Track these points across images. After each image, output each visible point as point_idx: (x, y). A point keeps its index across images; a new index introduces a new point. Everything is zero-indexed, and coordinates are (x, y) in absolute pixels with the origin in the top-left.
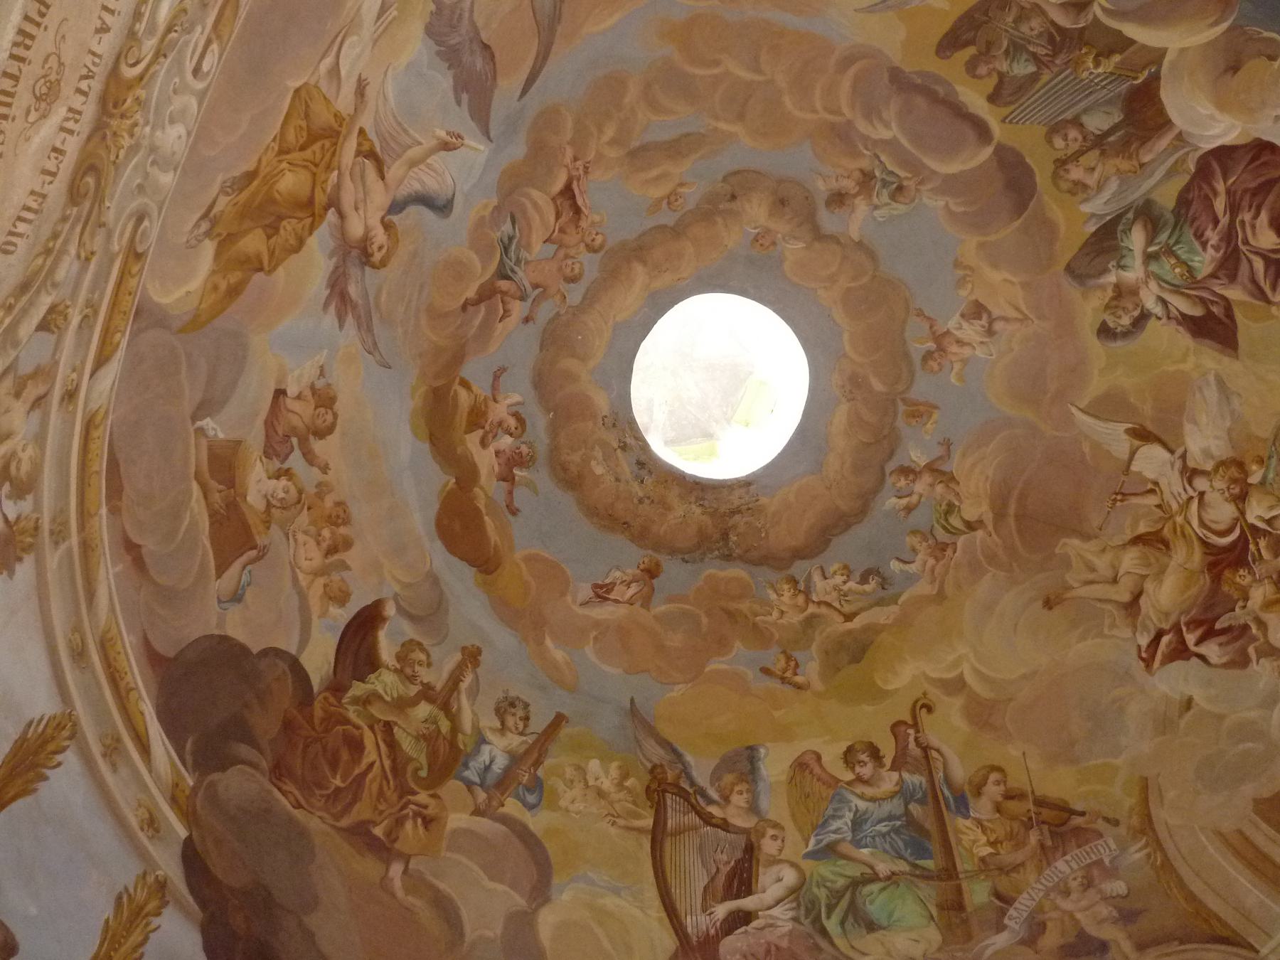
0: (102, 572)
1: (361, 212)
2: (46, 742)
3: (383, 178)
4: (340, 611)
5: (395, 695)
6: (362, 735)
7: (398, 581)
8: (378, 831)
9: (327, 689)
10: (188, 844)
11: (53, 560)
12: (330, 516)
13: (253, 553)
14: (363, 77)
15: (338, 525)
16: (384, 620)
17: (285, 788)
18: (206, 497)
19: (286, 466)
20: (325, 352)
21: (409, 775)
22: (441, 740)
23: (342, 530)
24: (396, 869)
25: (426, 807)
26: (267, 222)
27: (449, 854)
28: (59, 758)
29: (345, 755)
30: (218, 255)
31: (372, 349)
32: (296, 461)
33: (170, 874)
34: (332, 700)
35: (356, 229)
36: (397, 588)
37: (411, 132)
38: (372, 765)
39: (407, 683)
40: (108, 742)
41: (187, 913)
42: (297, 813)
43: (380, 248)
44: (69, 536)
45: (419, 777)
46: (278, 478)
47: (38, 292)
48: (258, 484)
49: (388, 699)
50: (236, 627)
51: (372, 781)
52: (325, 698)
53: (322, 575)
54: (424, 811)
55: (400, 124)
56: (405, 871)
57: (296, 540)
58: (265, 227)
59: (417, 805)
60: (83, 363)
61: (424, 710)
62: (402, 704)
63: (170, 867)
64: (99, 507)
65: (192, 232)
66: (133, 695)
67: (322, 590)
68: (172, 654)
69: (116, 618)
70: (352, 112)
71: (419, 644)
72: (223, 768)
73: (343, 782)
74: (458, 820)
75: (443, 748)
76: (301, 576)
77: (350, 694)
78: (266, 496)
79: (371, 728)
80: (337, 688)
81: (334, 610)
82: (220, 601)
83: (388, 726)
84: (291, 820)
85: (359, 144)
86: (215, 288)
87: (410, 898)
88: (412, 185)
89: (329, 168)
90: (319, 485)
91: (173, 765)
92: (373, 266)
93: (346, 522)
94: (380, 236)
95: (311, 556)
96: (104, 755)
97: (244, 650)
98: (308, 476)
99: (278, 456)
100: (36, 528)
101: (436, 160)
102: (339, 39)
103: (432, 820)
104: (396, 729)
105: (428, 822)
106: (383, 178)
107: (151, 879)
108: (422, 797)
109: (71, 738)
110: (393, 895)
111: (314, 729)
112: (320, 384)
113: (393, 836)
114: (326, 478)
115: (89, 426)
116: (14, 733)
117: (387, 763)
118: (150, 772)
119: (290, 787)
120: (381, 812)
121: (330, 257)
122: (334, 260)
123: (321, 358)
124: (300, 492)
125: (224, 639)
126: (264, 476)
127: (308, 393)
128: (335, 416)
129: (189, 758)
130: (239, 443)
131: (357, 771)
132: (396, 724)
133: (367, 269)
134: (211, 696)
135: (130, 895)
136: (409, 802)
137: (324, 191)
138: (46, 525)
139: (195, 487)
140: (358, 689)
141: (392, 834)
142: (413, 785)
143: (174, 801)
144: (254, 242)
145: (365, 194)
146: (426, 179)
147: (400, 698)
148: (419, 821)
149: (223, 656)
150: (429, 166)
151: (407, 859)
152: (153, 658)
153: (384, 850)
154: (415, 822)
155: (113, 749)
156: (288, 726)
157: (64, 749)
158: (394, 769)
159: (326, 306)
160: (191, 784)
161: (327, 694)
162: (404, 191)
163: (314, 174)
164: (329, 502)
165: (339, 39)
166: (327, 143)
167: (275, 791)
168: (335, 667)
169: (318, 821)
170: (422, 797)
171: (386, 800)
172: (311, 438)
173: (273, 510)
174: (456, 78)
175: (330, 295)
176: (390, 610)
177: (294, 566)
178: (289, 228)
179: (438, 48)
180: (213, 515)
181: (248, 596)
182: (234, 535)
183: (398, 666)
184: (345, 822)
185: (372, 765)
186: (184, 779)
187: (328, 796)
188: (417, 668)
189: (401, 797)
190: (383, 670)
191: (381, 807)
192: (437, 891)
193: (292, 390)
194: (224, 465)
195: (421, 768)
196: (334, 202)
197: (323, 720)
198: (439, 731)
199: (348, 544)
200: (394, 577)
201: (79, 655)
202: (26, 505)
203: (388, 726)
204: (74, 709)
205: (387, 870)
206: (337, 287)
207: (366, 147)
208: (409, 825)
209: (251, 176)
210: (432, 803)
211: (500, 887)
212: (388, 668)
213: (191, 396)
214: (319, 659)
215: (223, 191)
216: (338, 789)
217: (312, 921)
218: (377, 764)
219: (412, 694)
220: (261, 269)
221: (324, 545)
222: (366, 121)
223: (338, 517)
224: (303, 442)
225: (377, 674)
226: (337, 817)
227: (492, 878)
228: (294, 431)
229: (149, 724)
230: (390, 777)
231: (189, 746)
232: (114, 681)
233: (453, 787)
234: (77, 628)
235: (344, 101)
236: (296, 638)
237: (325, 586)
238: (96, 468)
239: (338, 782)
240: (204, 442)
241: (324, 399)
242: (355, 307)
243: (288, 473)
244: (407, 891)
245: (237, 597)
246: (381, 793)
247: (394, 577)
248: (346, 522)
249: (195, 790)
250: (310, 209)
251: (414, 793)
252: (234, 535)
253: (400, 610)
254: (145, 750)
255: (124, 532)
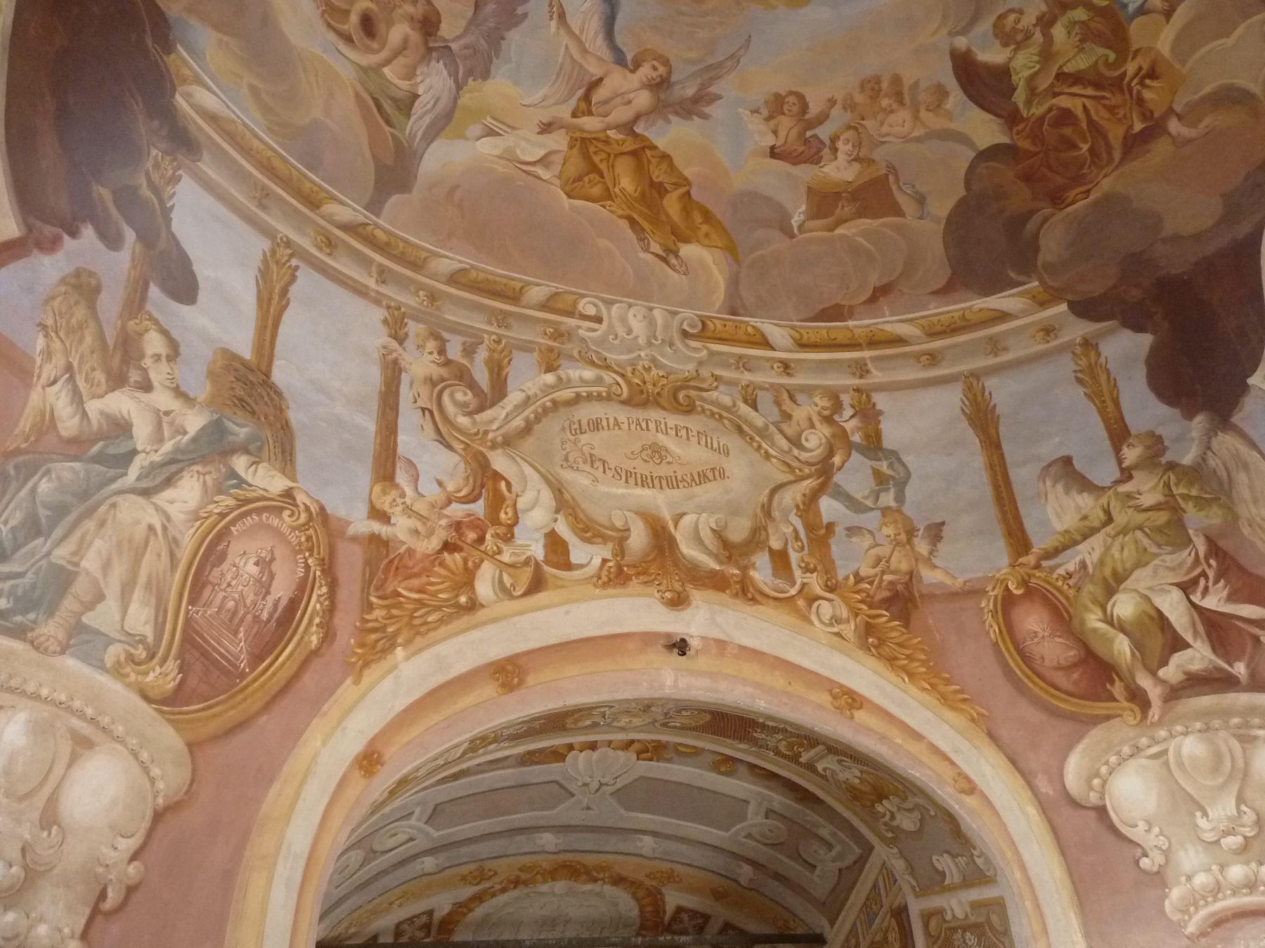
0: (888, 327)
1: (631, 96)
2: (975, 399)
3: (601, 80)
4: (951, 99)
5: (1037, 58)
6: (1059, 108)
7: (937, 30)
8: (1138, 127)
9: (1011, 129)
10: (1072, 306)
11: (877, 376)
12: (871, 97)
13: (891, 178)
14: (538, 130)
15: (880, 90)
16: (969, 51)
17: (1070, 200)
18: (845, 221)
19: (828, 142)
20: (740, 110)
21: (1108, 73)
22: (1092, 25)
23: (885, 85)
24: (1174, 126)
25: (1140, 69)
26: (656, 195)
27: (1188, 66)
28: (987, 393)
29: (1067, 131)
30: (687, 241)
31: (735, 58)
32: (824, 132)
33: (1081, 333)
34: (1021, 127)
35: (643, 99)
36: (945, 31)
37: (560, 60)
38: (1084, 106)
39: (1031, 41)
40: (989, 348)
41: (1112, 331)
42: (1092, 197)
43: (655, 69)
44: (864, 359)
45: (1113, 64)
46: (836, 150)
47: (739, 417)
48: (839, 170)
49: (1038, 67)
50: (942, 207)
51: (1097, 113)
52: (1018, 133)
53: (918, 111)
54: (1143, 72)
55: (558, 75)
56: (1179, 117)
57: (887, 135)
58: (662, 197)
59: (1134, 77)
60: (768, 359)
61: (1058, 32)
62: (1047, 54)
63: (1079, 329)
64: (847, 328)
65: (678, 272)
66: (968, 315)
67: (931, 114)
68: (949, 272)
69: (917, 319)
70: (564, 131)
71: (999, 17)
72: (1037, 250)
73: (1085, 142)
74: (1164, 42)
75: (1098, 25)
76: (916, 134)
77: (1021, 105)
78: (849, 162)
79: (1056, 95)
80: (1012, 119)
81: (949, 104)
82: (921, 218)
83: (1061, 76)
84: (1096, 203)
85: (584, 114)
86: (707, 235)
87: (1202, 125)
88: (598, 44)
89: (607, 141)
90: (845, 108)
91: (1020, 294)
92: (670, 73)
93: (877, 80)
94: (645, 71)
95: (900, 121)
96: (996, 355)
97: (962, 203)
98: (839, 117)
99: (819, 150)
100: (858, 390)
101: (574, 22)
102: (524, 167)
103: (1153, 70)
104: (1066, 70)
105: (1152, 74)
106: (601, 80)
107: (1078, 350)
108: (1131, 68)
109: (978, 379)
110: (1189, 141)
111: (1036, 154)
112: (765, 113)
113: (1148, 114)
114: (839, 102)
115: (803, 345)
116: (964, 424)
117: (1090, 91)
118: (1017, 318)
119: (1072, 194)
120: (1125, 116)
121: (669, 122)
122: (671, 117)
123: (744, 112)
124: (849, 127)
125: (949, 220)
126: (834, 164)
127: (772, 123)
128: (791, 93)
129: (1021, 278)
130: (810, 190)
131: (1084, 125)
132: (1061, 67)
133: (674, 78)
134: (987, 244)
135: (1080, 371)
136: (1129, 84)
137: (624, 141)
138: (856, 382)
139: (840, 231)
140: (1020, 97)
141: (1146, 115)
142: (1117, 73)
143: (1043, 305)
144: (672, 204)
145: (618, 96)
146: (591, 35)
147: (1040, 54)
148: (1148, 81)
149: (961, 224)
150: (582, 31)
151: (1171, 111)
152: (946, 291)
153: (1154, 129)
154: (1148, 87)
155: (995, 345)
156: (1028, 178)
157: (983, 387)
158: (1097, 86)
159: (705, 117)
160: (1037, 283)
161: (1015, 130)
162: (606, 54)
163: (616, 156)
164: (859, 98)
165: (524, 167)
166: (592, 149)
167: (1070, 209)
168: (996, 115)
169: (1106, 180)
170: (1131, 68)
171: (1118, 107)
172: (807, 117)
173: (861, 155)
174: (508, 29)
175: (696, 114)
176: (961, 42)
177: (907, 139)
178: (657, 173)
179: (495, 60)
180: (859, 215)
181: (922, 189)
182: (873, 196)
183: (1013, 47)
184: (1117, 155)
185: (1084, 106)
186: (1031, 289)
187: (1093, 162)
188: (1020, 26)
189: (1122, 92)
190: (1013, 64)
191: (1121, 115)
192: (1208, 98)
193: (770, 140)
194: (824, 202)
195: (1107, 57)
196: (628, 128)
197: (1034, 143)
198: (1083, 22)
199: (897, 80)
200: (934, 34)
201: (933, 358)
202: (846, 399)
203: (1061, 76)
204: (961, 373)
205: (1170, 135)
206: (692, 107)
207: (583, 106)
208: (1147, 95)
209: (633, 223)
210: (1139, 60)
211: (1240, 30)
212: (1011, 59)
213: (779, 243)
214: (985, 130)
215: (647, 250)
216: (1091, 150)
217: (1168, 230)
218: (1088, 103)
219: (1041, 39)
220: (688, 193)
221: (895, 106)
222: (564, 112)
223: (873, 89)
224: (811, 125)
225: (1013, 73)
226: (1111, 160)
227: (1228, 35)
228: (801, 134)
229: (991, 306)
230: (1099, 94)
231: (1013, 275)
232: (953, 330)
233: (1137, 30)
234: (917, 356)
235: (558, 141)
236: (963, 148)
237: (928, 110)
238: (824, 332)
239: (1085, 147)
240: (811, 224)
241: (776, 106)
242: (703, 86)
243: (834, 139)
244: (1193, 125)
245: (921, 200)
246: (1111, 109)
247: (934, 34)
248: (877, 80)
249: (1042, 282)
250: (641, 153)
251: (1125, 74)
252: (873, 196)
253: (964, 32)
254: (1003, 316)
255: (865, 303)
